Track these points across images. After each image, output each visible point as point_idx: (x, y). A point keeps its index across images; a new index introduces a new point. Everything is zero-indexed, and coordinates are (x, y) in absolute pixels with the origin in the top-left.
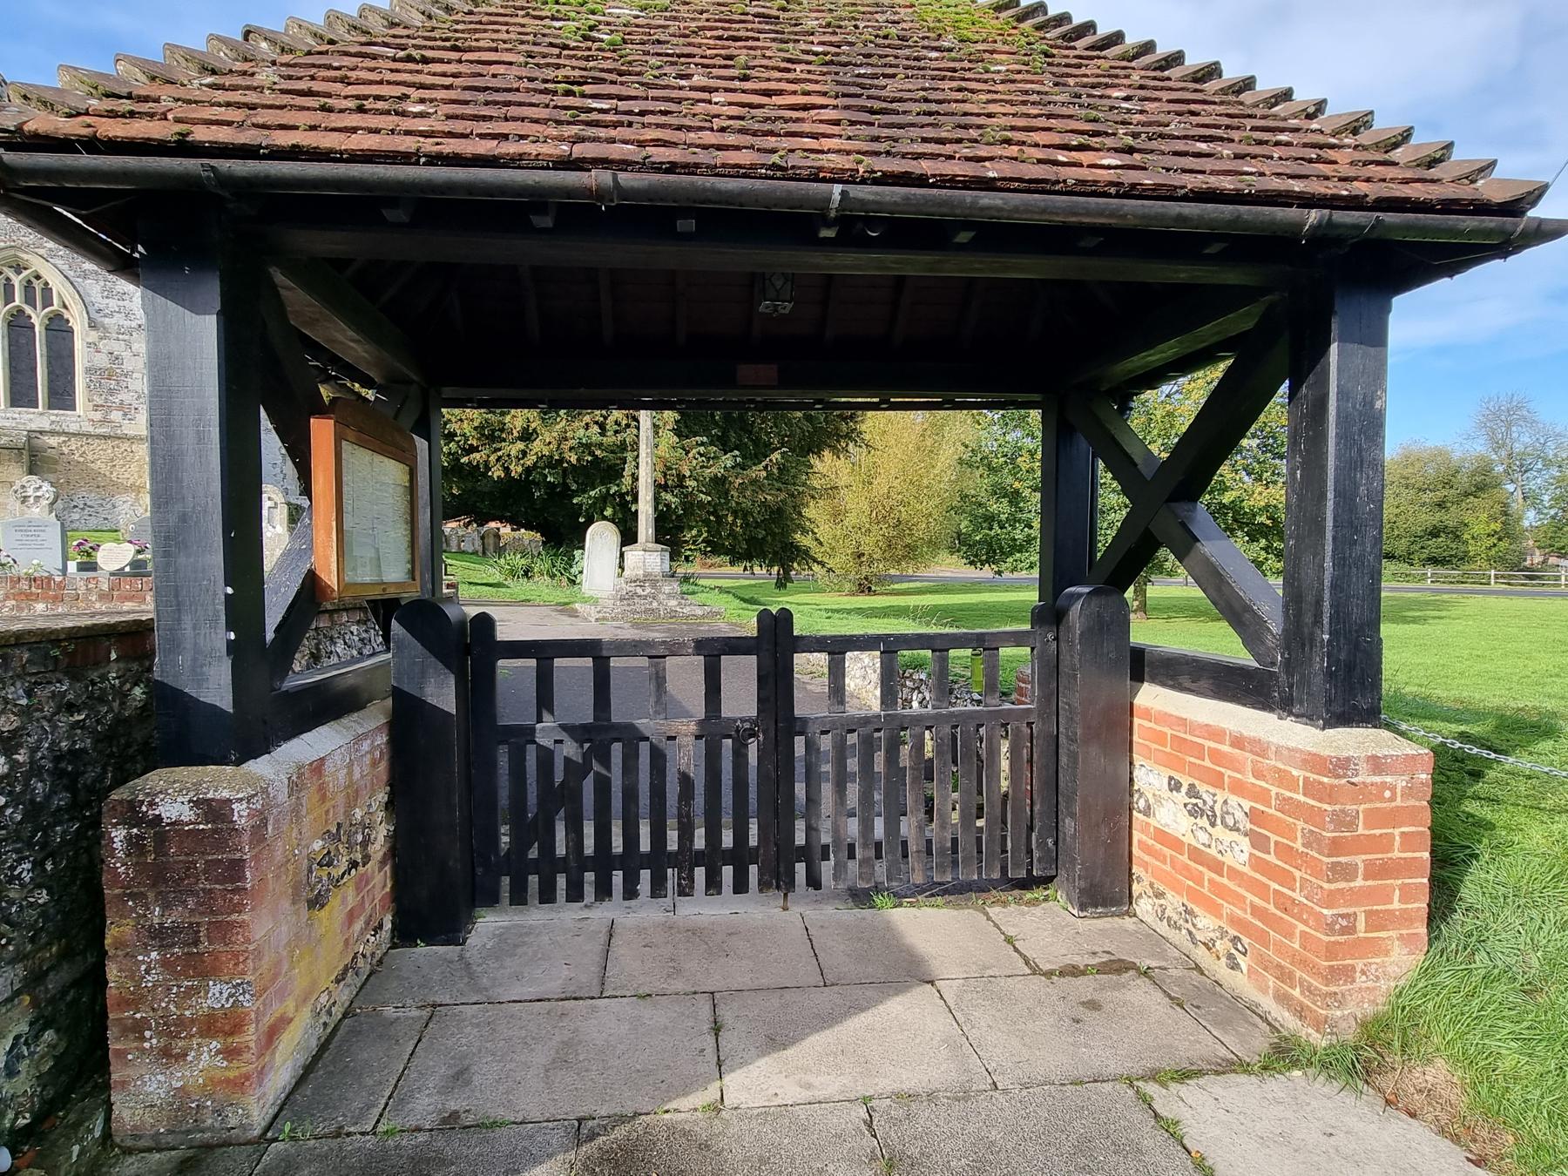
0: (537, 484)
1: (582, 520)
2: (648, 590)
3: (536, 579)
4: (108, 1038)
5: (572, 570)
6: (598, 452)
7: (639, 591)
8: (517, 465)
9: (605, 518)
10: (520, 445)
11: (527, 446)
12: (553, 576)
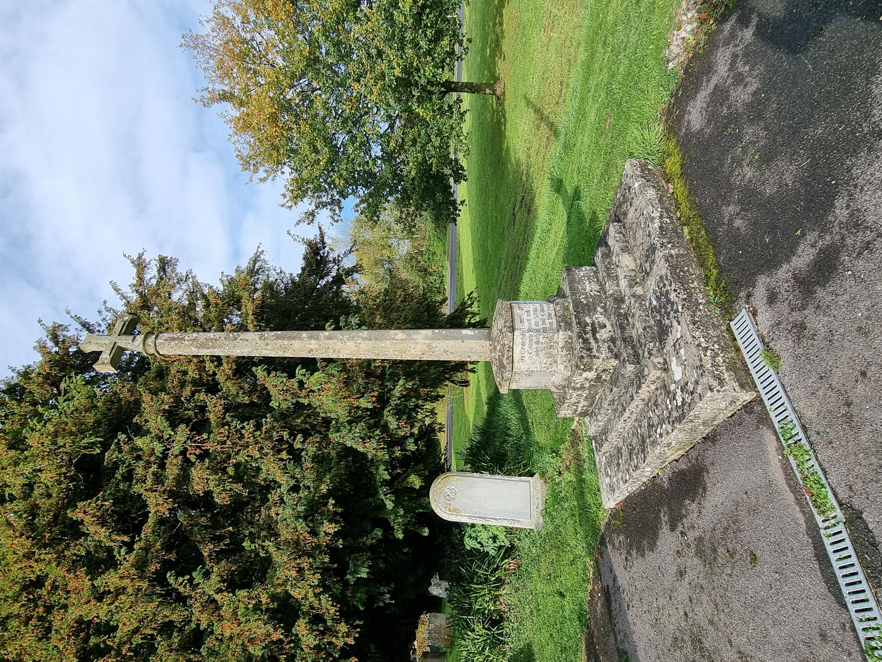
0: (371, 600)
1: (426, 532)
2: (599, 317)
3: (503, 608)
4: (352, 447)
5: (492, 553)
6: (324, 488)
7: (603, 334)
8: (335, 634)
9: (425, 491)
10: (301, 627)
11: (305, 614)
12: (500, 582)
